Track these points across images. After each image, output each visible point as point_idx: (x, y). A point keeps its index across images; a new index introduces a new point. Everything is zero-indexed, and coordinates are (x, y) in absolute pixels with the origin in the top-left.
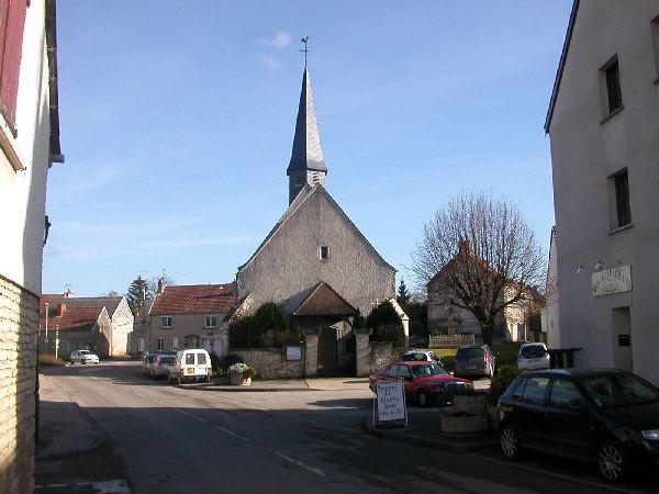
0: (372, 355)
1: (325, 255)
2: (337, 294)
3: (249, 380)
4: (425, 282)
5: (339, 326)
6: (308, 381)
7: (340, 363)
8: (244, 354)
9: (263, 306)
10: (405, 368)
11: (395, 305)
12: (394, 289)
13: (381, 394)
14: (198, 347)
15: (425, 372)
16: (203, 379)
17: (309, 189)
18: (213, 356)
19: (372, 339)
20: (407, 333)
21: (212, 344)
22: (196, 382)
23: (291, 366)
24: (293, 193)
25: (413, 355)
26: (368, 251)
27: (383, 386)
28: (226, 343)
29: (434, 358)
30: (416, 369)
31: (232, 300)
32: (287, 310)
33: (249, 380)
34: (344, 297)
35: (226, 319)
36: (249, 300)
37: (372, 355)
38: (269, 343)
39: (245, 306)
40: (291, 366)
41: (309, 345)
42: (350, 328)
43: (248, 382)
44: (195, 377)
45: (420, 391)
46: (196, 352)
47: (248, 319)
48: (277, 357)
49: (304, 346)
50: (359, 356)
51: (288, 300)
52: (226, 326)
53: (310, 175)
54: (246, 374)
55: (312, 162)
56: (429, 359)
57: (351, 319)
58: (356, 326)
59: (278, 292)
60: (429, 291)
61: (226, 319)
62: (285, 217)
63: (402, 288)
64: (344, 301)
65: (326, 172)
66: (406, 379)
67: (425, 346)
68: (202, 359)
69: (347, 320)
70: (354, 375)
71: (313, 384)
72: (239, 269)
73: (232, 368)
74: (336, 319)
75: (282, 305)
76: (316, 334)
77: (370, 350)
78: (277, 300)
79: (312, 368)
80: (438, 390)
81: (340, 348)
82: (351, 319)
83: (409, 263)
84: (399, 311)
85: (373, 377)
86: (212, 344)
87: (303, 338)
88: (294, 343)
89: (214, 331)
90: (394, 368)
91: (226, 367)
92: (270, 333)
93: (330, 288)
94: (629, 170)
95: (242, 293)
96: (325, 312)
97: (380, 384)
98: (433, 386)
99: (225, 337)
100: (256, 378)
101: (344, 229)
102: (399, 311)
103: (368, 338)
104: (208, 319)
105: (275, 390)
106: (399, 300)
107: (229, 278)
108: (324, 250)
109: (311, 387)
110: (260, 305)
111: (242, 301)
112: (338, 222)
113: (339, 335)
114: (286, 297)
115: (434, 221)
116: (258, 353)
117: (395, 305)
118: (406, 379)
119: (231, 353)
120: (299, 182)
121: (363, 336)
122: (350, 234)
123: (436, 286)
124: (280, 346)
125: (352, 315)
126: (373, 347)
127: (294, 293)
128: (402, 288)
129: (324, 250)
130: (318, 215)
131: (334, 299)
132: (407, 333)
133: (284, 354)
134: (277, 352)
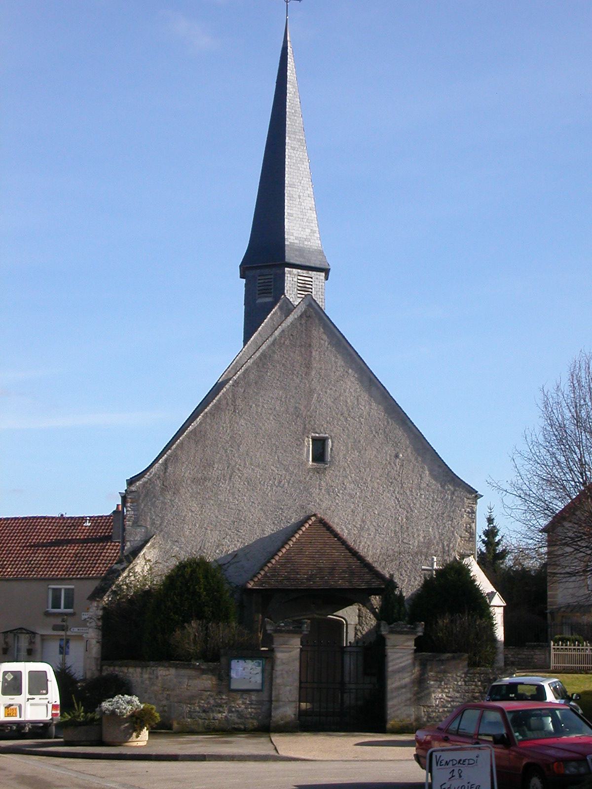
0: (420, 683)
1: (320, 455)
2: (343, 542)
3: (145, 733)
4: (544, 523)
5: (349, 615)
6: (276, 738)
7: (349, 699)
8: (134, 674)
9: (182, 567)
10: (493, 716)
11: (477, 572)
12: (472, 535)
13: (441, 775)
14: (31, 656)
15: (542, 727)
16: (39, 730)
17: (288, 308)
18: (63, 678)
19: (421, 645)
20: (500, 633)
21: (63, 650)
22: (24, 736)
23: (240, 704)
24: (251, 325)
25: (513, 687)
26: (416, 450)
27: (446, 756)
28: (95, 649)
29: (560, 693)
30: (521, 720)
31: (111, 551)
32: (234, 576)
33: (145, 733)
34: (362, 552)
35: (97, 594)
36: (149, 553)
37: (420, 683)
38: (192, 649)
39: (140, 566)
40: (240, 704)
41: (280, 655)
42: (374, 622)
43: (142, 740)
44: (20, 725)
45: (532, 769)
46: (25, 668)
47: (145, 596)
48: (207, 682)
49: (268, 659)
50: (393, 683)
51: (235, 555)
52: (94, 611)
53: (292, 279)
54: (137, 721)
55: (301, 251)
56: (550, 697)
57: (376, 600)
58: (388, 615)
59: (213, 537)
60: (551, 543)
61: (97, 594)
62: (235, 368)
63: (491, 533)
64: (361, 559)
65: (326, 271)
66: (498, 741)
67: (544, 668)
68: (38, 684)
69: (365, 602)
70: (382, 730)
71: (287, 745)
72: (131, 482)
73: (106, 705)
74: (343, 598)
75: (221, 566)
76: (296, 629)
77: (417, 670)
78: (212, 556)
79: (287, 711)
80: (571, 769)
81: (350, 663)
82: (376, 600)
83: (507, 476)
84: (485, 585)
85: (422, 735)
86: (63, 650)
87: (268, 640)
88: (248, 652)
89: (70, 621)
90: (471, 715)
91: (93, 704)
92: (194, 626)
93: (329, 528)
94: (87, 597)
95: (134, 537)
96: (318, 584)
97: (443, 751)
98: (565, 761)
99: (93, 635)
100: (161, 729)
101: (365, 396)
102: (485, 585)
103: (411, 644)
104: (57, 592)
105: (202, 758)
106: (482, 561)
107: (106, 506)
108: (320, 445)
109: (283, 753)
110: (174, 563)
111: (135, 552)
112: (351, 386)
113: (350, 637)
114: (232, 546)
115: (566, 387)
116: (166, 674)
117: (477, 572)
118: (498, 741)
119: (108, 671)
120: (265, 292)
121: (402, 638)
122: (376, 411)
123: (569, 529)
124: (216, 658)
125: (375, 592)
126: (423, 665)
127: (249, 540)
128: (491, 533)
129: (320, 445)
130: (308, 366)
131: (338, 554)
132: (500, 633)
133: (224, 677)
134: (212, 671)
